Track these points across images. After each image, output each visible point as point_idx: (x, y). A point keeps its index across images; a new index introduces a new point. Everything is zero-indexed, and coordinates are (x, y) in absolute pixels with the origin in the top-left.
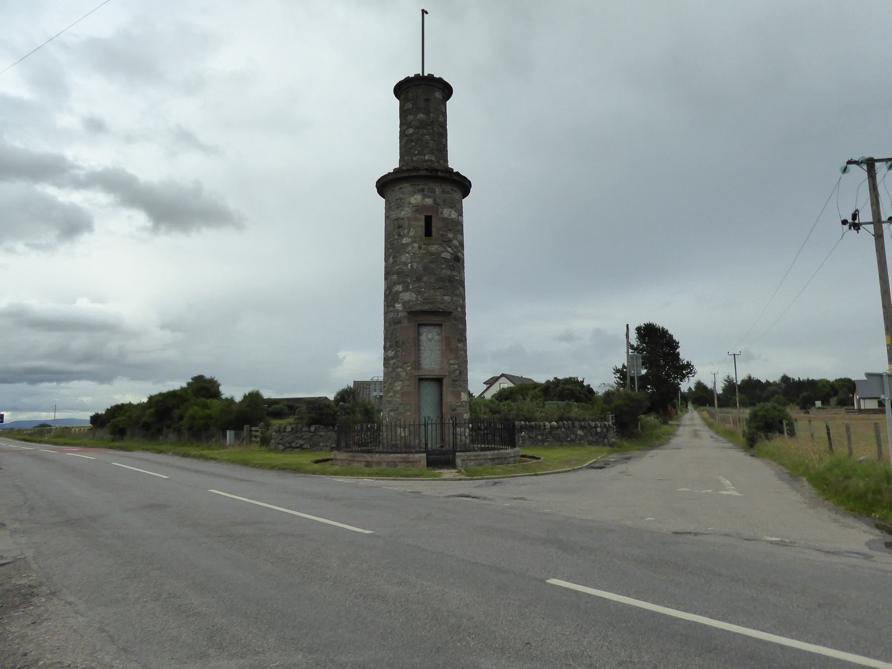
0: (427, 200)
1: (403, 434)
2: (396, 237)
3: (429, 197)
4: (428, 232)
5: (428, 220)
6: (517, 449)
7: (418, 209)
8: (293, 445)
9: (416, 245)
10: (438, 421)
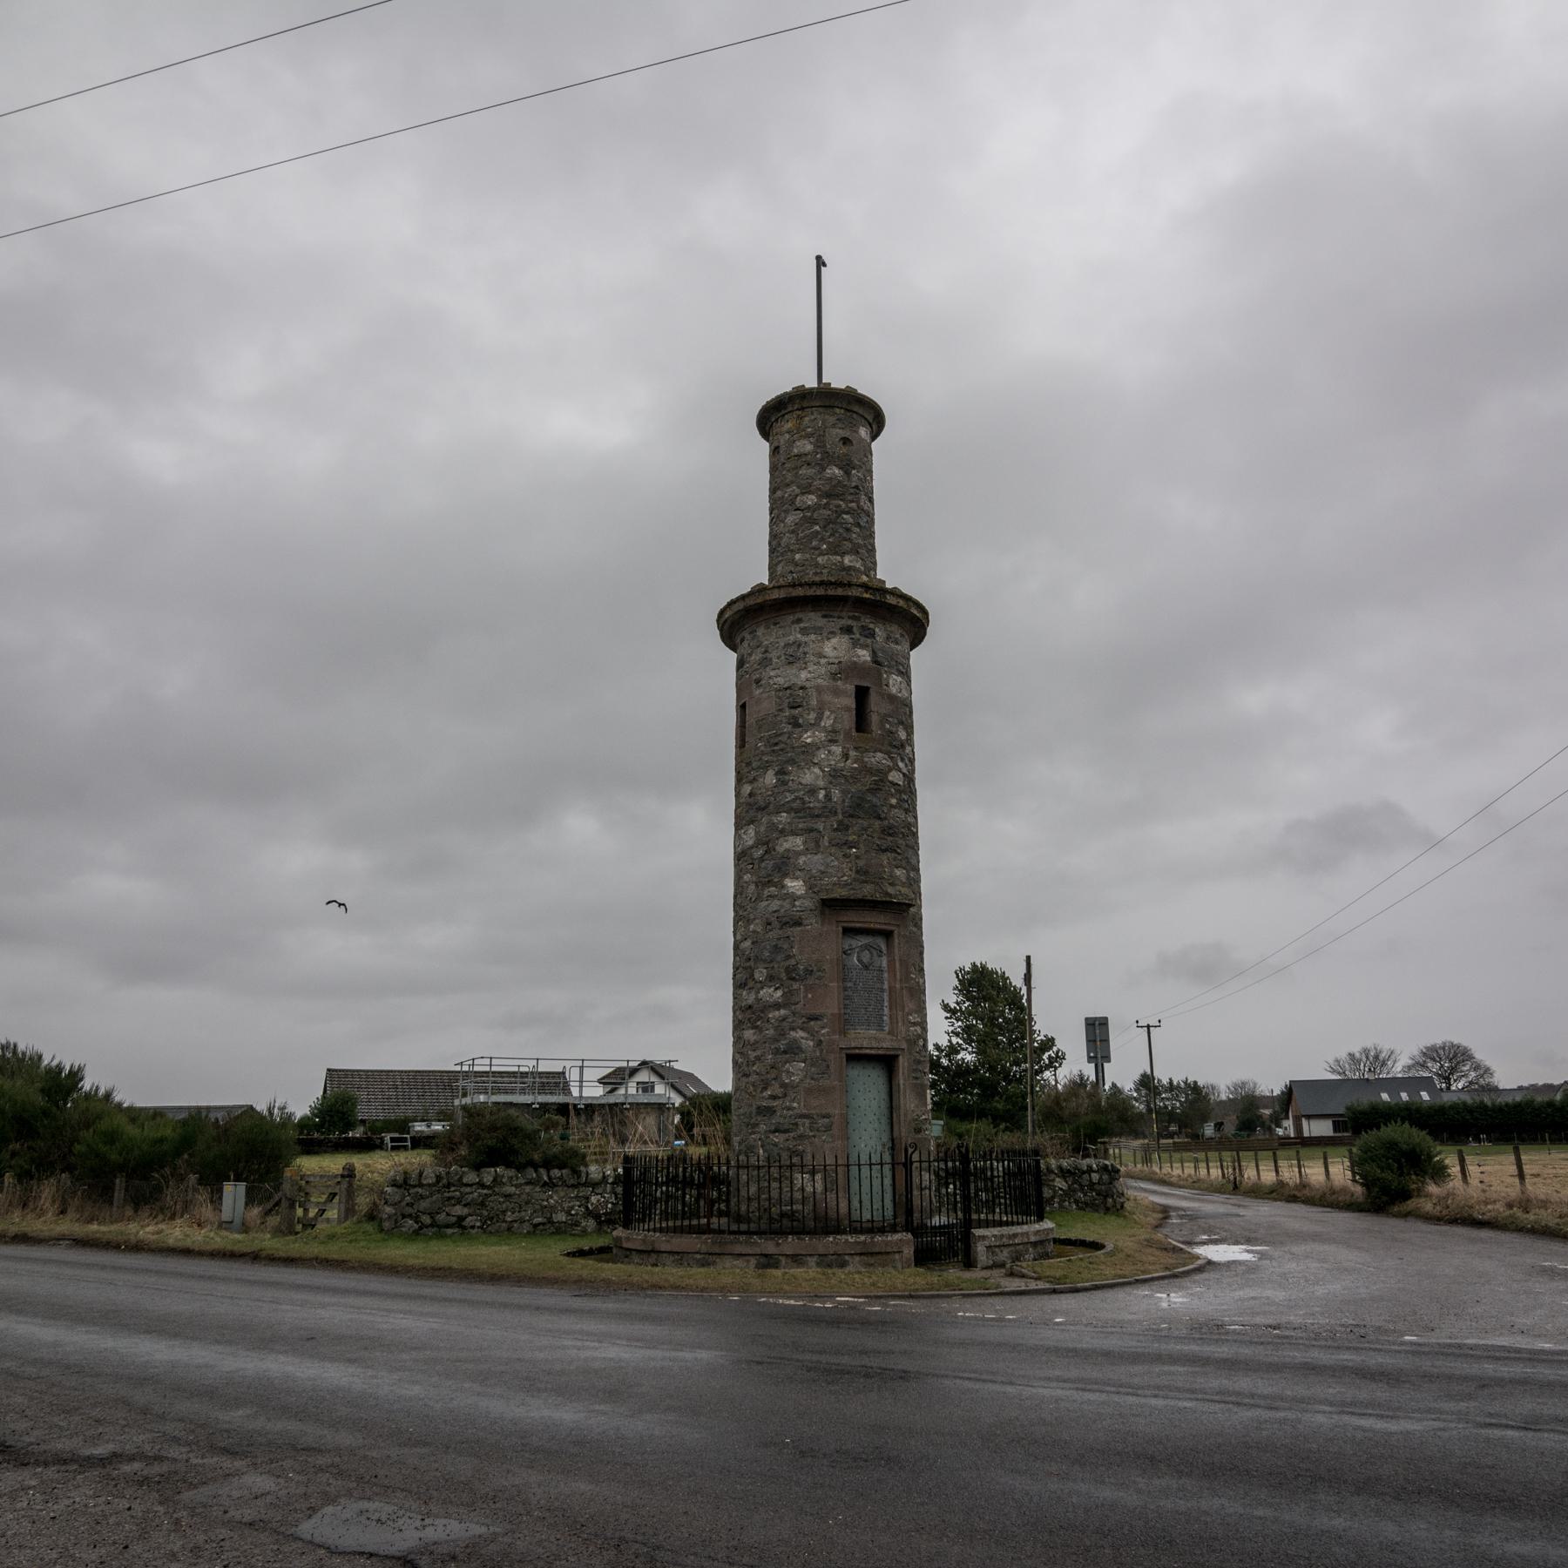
0: (862, 652)
1: (809, 1189)
3: (864, 647)
4: (861, 723)
5: (862, 694)
6: (1048, 1224)
7: (843, 671)
8: (441, 1217)
9: (837, 749)
10: (887, 1158)
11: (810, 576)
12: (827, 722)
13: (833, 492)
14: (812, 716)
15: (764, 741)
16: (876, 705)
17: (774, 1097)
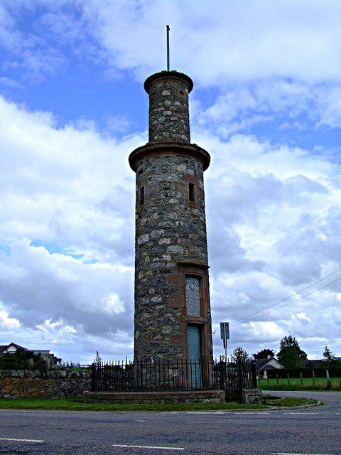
2: (163, 197)
3: (192, 169)
5: (191, 186)
9: (182, 206)
11: (169, 140)
12: (179, 196)
13: (178, 111)
14: (173, 193)
15: (146, 202)
16: (195, 190)
17: (158, 339)
